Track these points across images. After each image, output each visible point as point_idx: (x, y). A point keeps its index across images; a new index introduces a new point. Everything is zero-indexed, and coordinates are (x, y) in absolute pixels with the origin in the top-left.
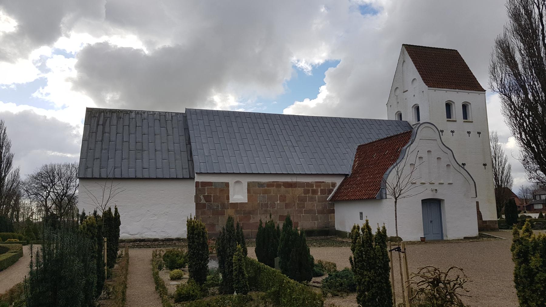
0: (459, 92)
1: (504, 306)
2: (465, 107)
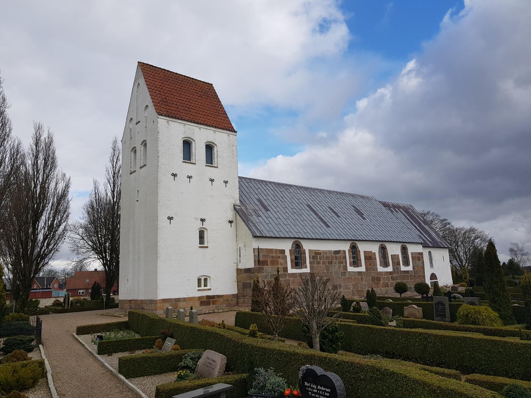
0: (216, 132)
1: (164, 397)
2: (209, 148)
